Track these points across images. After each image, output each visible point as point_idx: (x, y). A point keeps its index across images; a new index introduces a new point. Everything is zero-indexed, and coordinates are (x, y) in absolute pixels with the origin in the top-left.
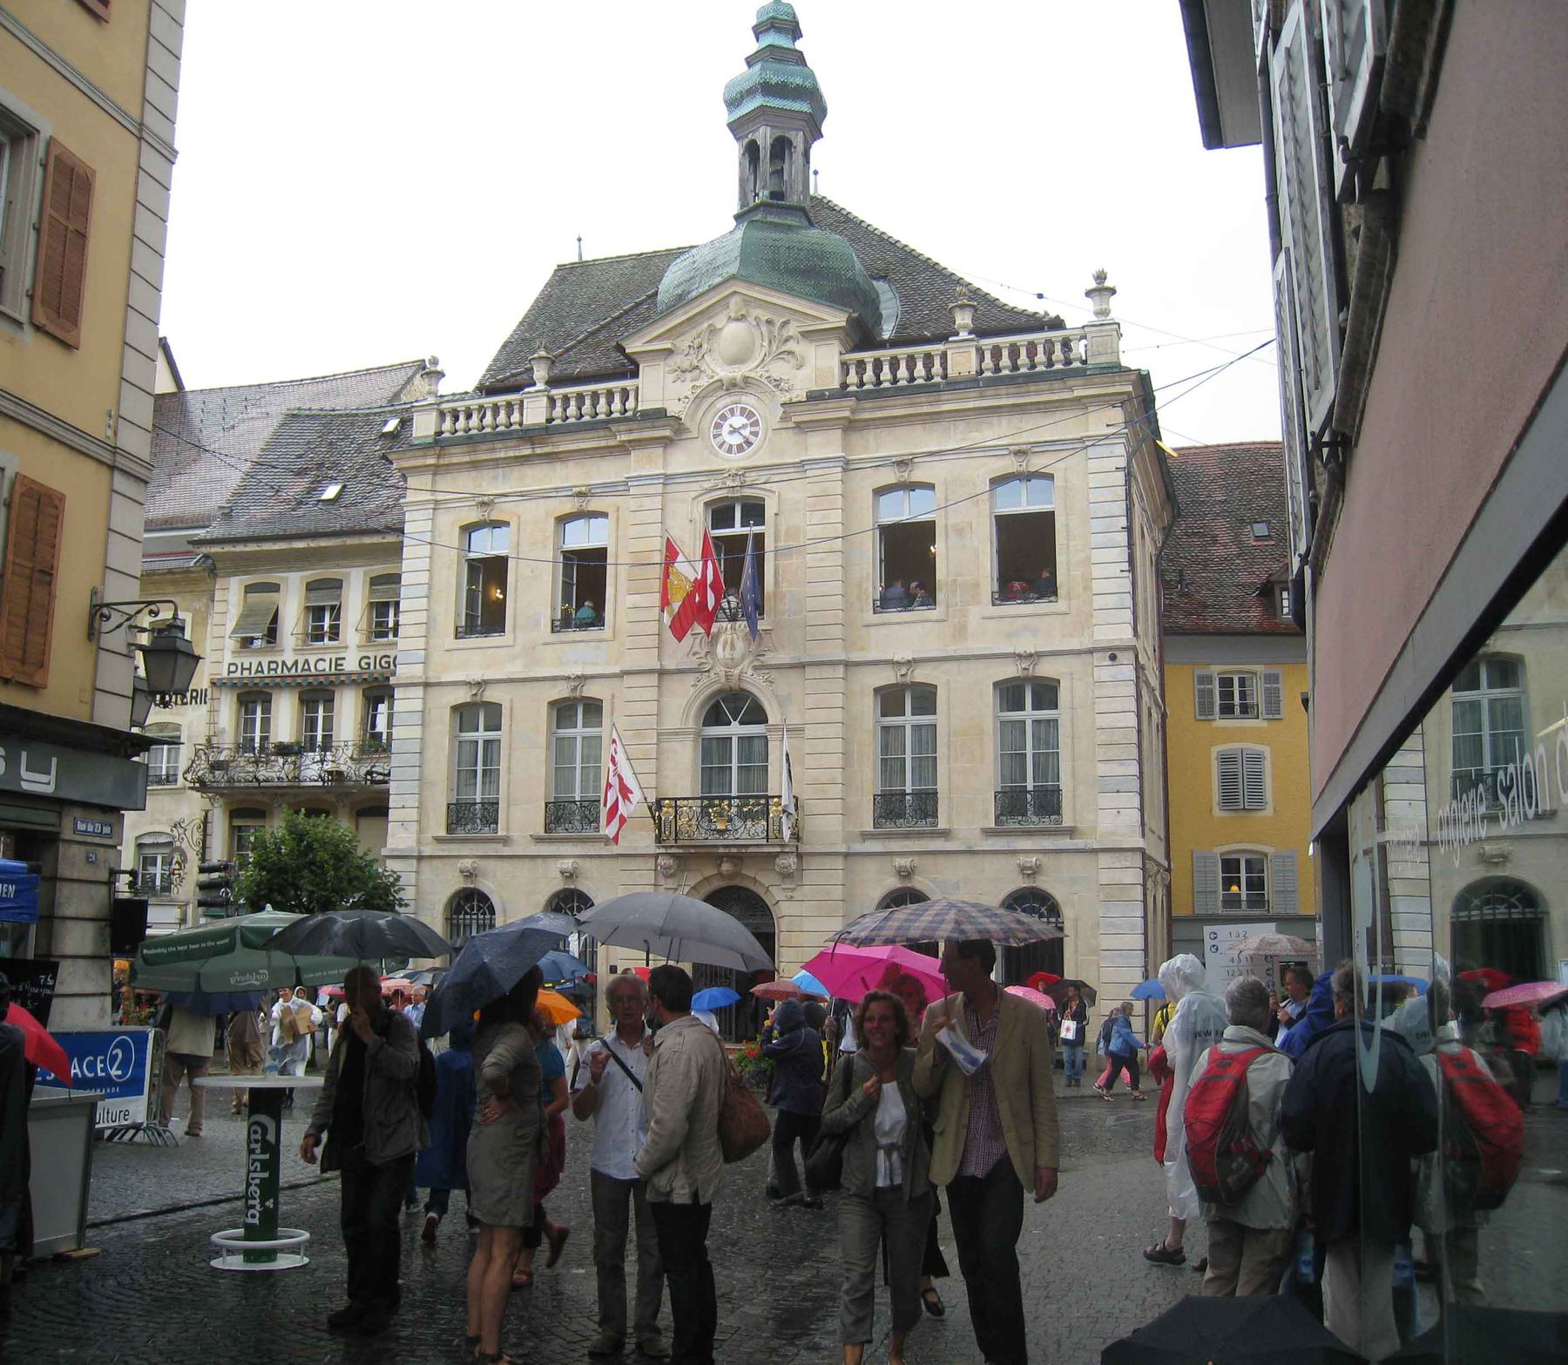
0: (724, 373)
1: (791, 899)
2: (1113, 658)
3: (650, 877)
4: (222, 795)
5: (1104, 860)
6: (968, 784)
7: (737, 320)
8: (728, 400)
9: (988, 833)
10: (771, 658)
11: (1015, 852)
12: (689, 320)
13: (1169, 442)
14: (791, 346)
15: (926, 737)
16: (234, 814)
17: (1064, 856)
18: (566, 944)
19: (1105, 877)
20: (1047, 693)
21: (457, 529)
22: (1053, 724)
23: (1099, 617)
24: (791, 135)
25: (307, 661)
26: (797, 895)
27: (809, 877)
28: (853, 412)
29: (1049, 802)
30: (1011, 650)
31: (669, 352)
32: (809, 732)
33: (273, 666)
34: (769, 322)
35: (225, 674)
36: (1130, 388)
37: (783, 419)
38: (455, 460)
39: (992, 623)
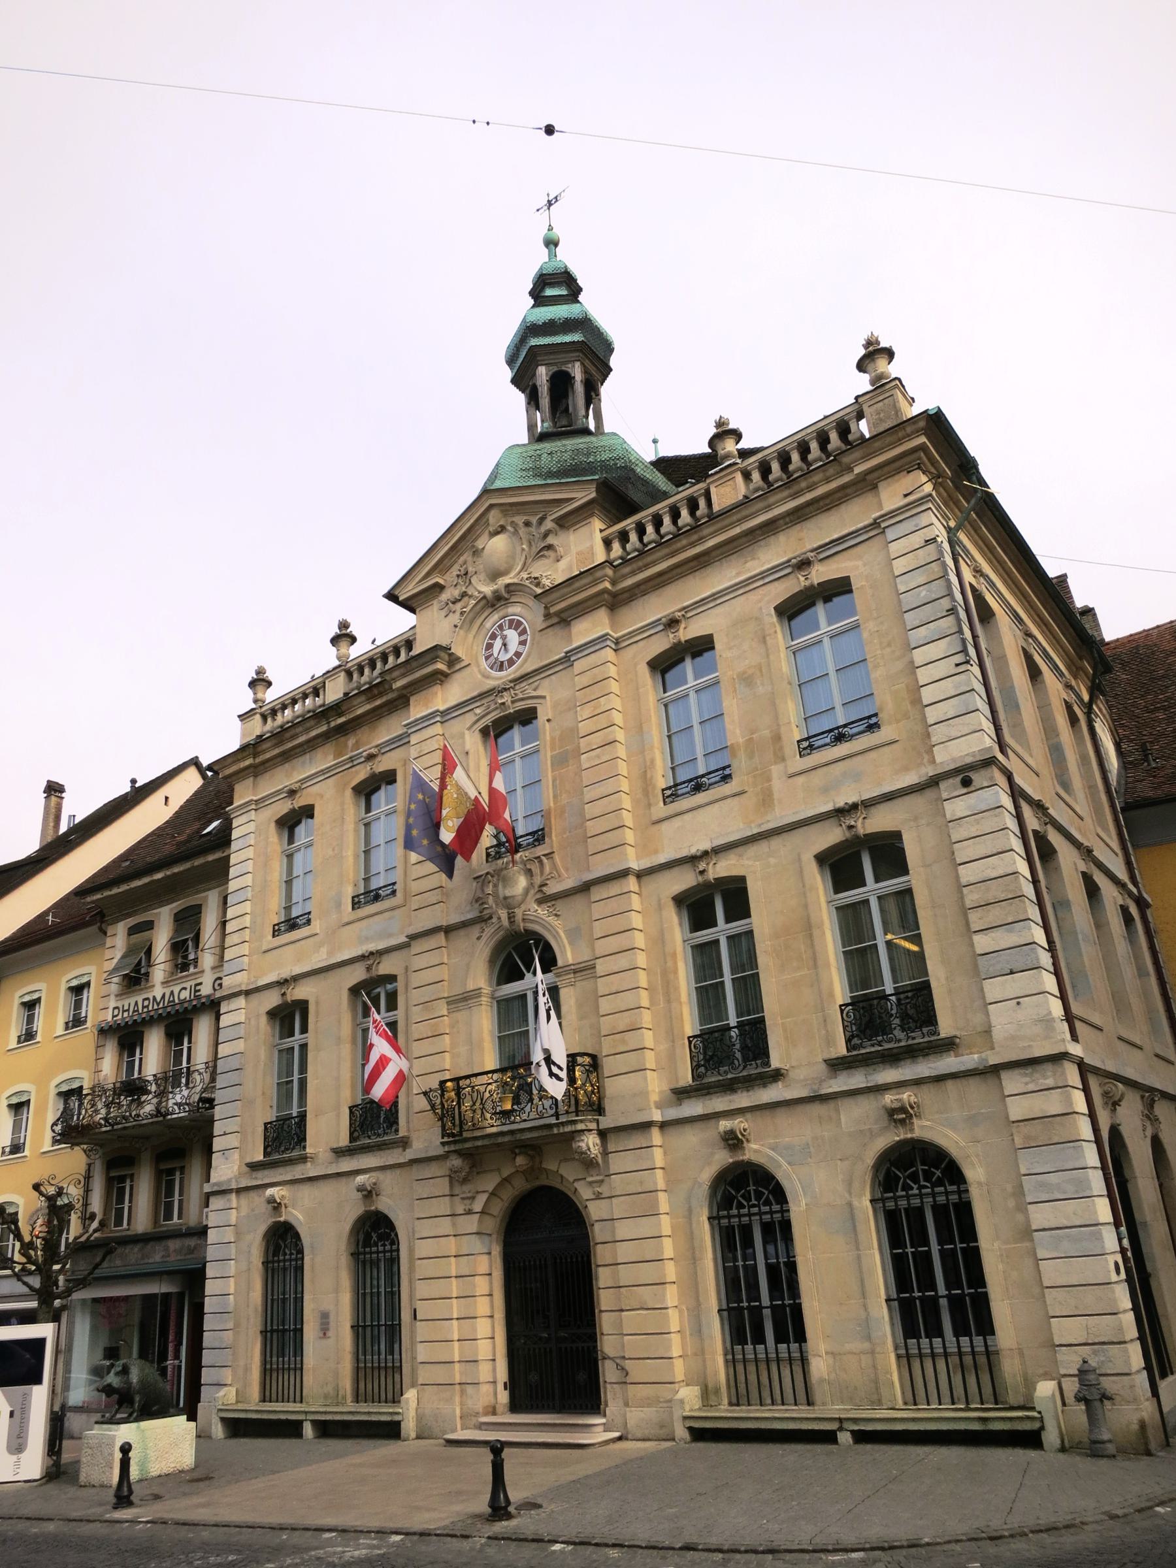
0: (487, 589)
1: (598, 1196)
2: (967, 782)
3: (443, 1186)
4: (101, 1146)
5: (1012, 1082)
6: (805, 1000)
7: (497, 533)
8: (496, 617)
9: (836, 1065)
10: (553, 888)
11: (879, 1089)
12: (453, 548)
13: (1114, 627)
14: (551, 540)
15: (744, 945)
16: (110, 1165)
17: (950, 1084)
18: (151, 1406)
19: (1017, 1109)
20: (889, 853)
21: (273, 825)
22: (906, 894)
23: (938, 734)
24: (568, 368)
25: (172, 993)
26: (604, 1190)
27: (617, 1163)
28: (613, 583)
29: (919, 1004)
30: (829, 807)
31: (438, 588)
32: (601, 967)
33: (146, 1003)
34: (527, 524)
35: (110, 1018)
36: (923, 439)
37: (547, 616)
38: (268, 755)
39: (800, 780)
